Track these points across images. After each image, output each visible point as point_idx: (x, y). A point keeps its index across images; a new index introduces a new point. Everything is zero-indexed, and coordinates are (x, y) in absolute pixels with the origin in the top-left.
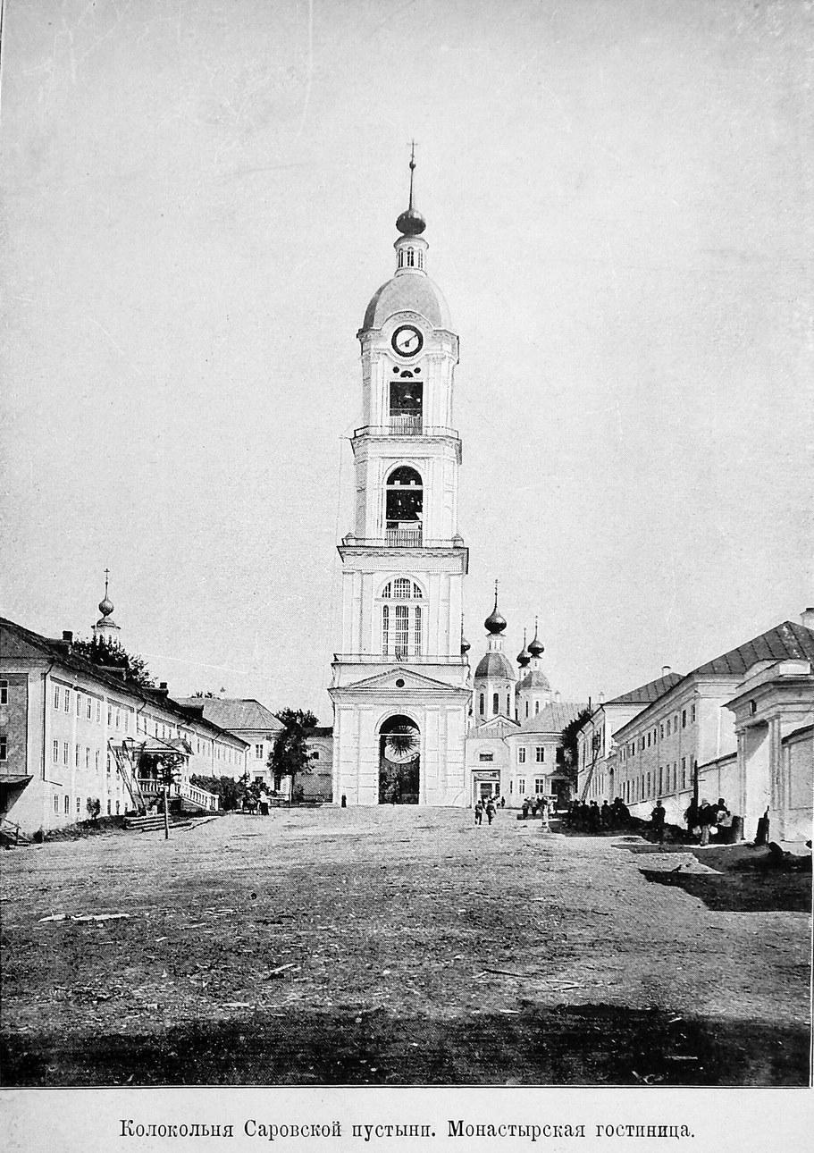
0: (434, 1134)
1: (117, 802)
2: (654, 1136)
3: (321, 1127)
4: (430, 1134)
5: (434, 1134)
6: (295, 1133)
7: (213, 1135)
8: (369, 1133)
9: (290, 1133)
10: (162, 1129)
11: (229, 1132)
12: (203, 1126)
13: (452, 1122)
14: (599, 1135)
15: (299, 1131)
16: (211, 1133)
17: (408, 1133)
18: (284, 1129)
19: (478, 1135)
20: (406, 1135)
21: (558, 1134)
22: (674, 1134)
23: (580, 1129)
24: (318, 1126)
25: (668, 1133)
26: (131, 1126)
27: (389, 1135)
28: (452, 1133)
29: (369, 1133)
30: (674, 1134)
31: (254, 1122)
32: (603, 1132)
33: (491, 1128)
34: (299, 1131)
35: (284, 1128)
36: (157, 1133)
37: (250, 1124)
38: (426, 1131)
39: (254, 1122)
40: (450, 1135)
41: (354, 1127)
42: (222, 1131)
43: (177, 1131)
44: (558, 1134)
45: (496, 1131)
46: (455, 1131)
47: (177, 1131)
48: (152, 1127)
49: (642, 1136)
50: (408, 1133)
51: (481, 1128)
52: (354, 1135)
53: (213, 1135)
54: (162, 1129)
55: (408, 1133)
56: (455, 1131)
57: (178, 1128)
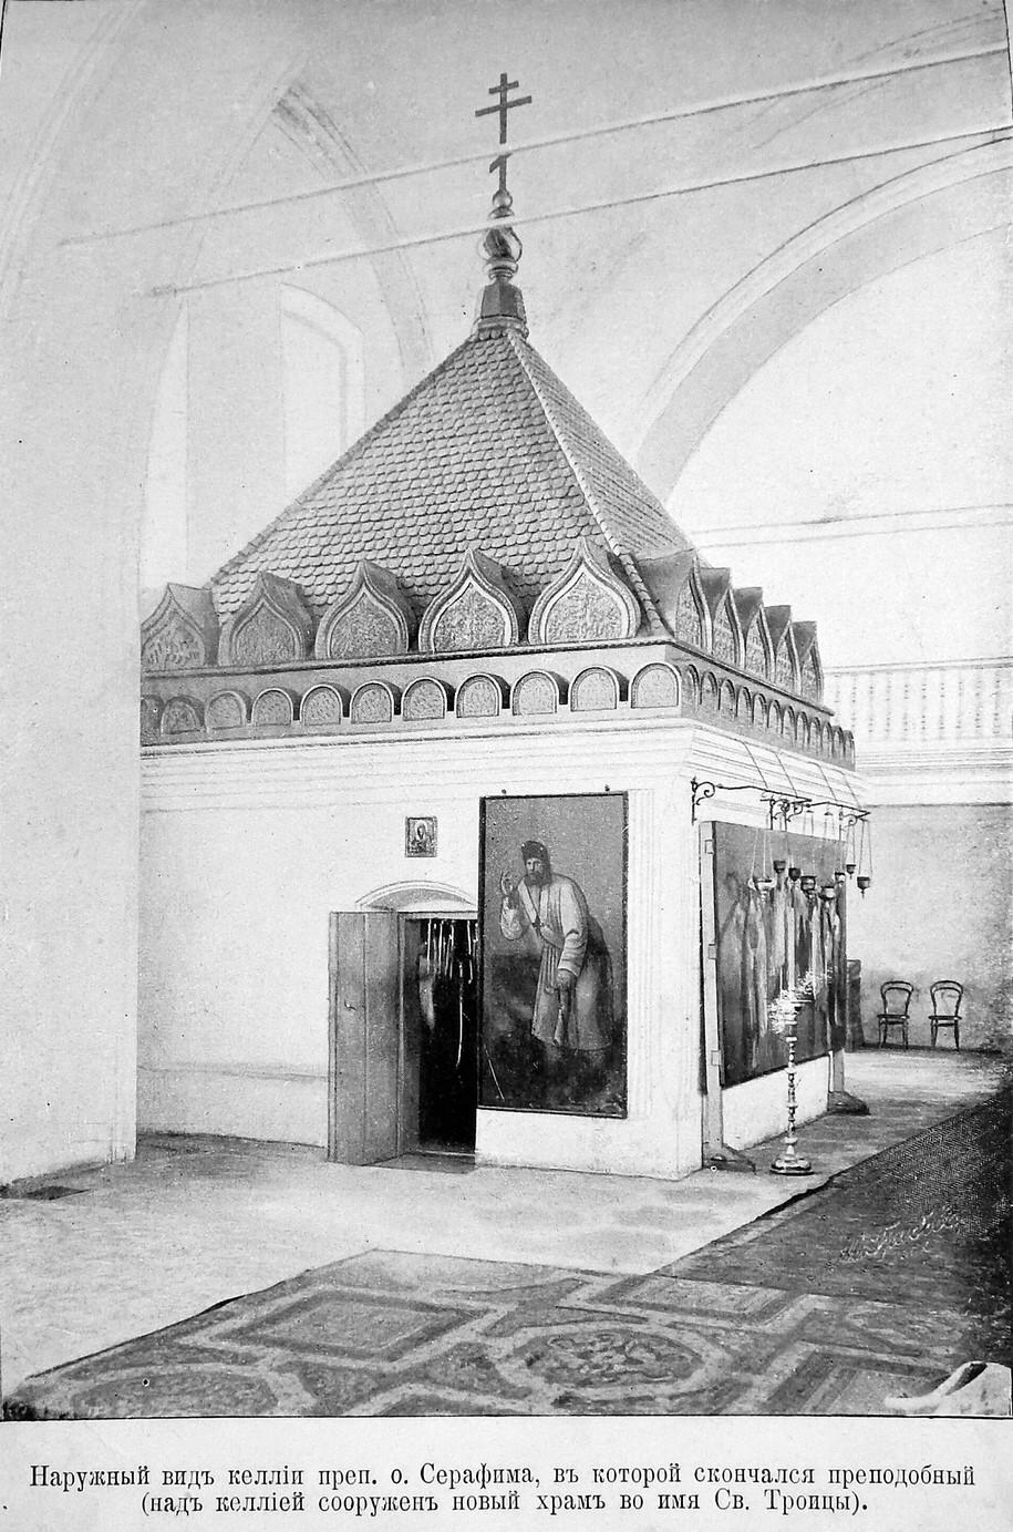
0: (865, 1507)
1: (966, 1477)
2: (942, 1482)
4: (370, 1481)
5: (374, 1482)
6: (485, 1505)
8: (82, 1482)
9: (479, 1506)
10: (472, 1504)
12: (757, 1481)
15: (631, 1502)
17: (507, 1505)
19: (737, 1481)
20: (504, 1508)
21: (713, 1478)
22: (828, 1506)
23: (808, 1473)
24: (238, 1472)
25: (821, 1505)
27: (624, 1480)
29: (82, 1482)
30: (828, 1506)
33: (527, 1472)
34: (631, 1502)
36: (907, 1480)
37: (428, 1469)
38: (503, 141)
41: (321, 1472)
42: (686, 1502)
43: (604, 1475)
44: (713, 1478)
47: (604, 1475)
48: (782, 1472)
49: (817, 1508)
50: (507, 1506)
51: (740, 1472)
52: (367, 1472)
54: (472, 1504)
55: (507, 1505)
57: (605, 1473)
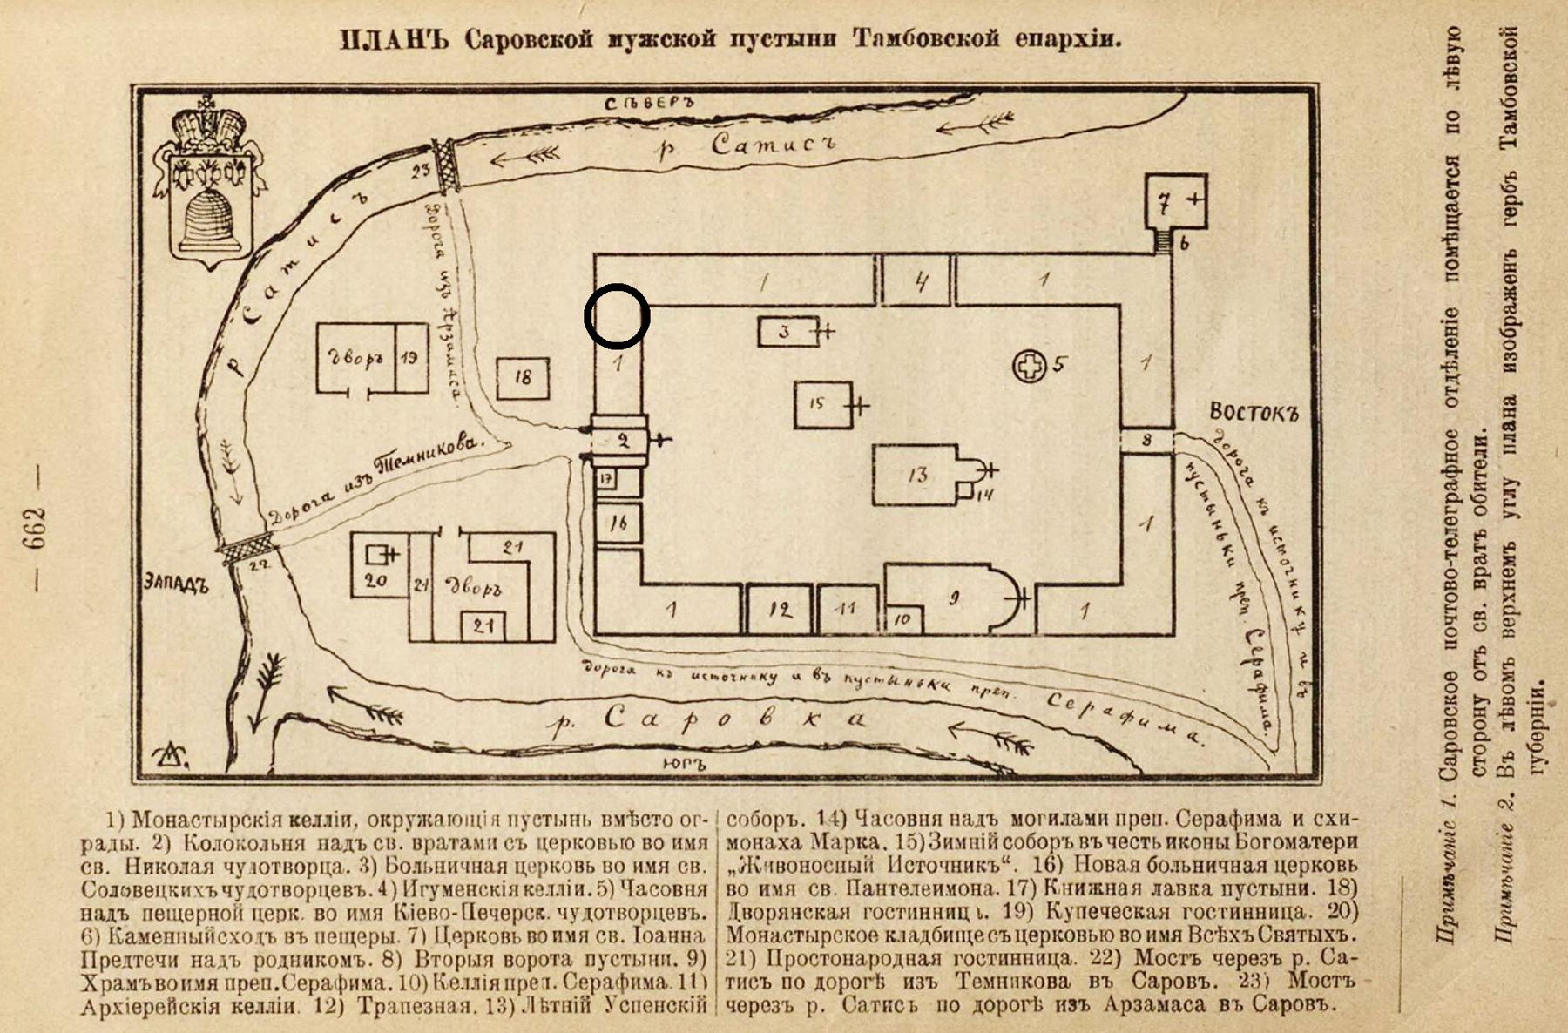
3: (247, 841)
7: (1195, 871)
11: (1452, 161)
13: (815, 834)
14: (111, 826)
15: (613, 866)
16: (1192, 869)
17: (1285, 892)
18: (1014, 1004)
26: (195, 840)
28: (731, 940)
30: (1455, 219)
31: (1188, 812)
32: (870, 914)
34: (613, 866)
35: (1449, 735)
39: (1188, 812)
40: (135, 827)
45: (1182, 1006)
46: (734, 938)
53: (1195, 871)
55: (1285, 892)
56: (818, 844)
